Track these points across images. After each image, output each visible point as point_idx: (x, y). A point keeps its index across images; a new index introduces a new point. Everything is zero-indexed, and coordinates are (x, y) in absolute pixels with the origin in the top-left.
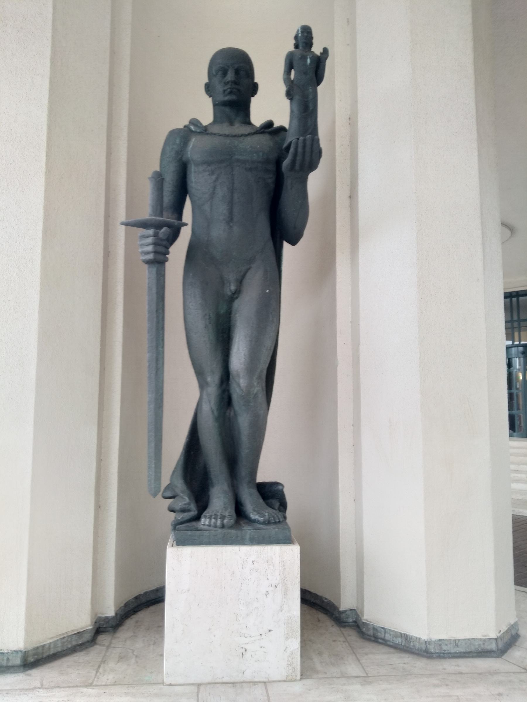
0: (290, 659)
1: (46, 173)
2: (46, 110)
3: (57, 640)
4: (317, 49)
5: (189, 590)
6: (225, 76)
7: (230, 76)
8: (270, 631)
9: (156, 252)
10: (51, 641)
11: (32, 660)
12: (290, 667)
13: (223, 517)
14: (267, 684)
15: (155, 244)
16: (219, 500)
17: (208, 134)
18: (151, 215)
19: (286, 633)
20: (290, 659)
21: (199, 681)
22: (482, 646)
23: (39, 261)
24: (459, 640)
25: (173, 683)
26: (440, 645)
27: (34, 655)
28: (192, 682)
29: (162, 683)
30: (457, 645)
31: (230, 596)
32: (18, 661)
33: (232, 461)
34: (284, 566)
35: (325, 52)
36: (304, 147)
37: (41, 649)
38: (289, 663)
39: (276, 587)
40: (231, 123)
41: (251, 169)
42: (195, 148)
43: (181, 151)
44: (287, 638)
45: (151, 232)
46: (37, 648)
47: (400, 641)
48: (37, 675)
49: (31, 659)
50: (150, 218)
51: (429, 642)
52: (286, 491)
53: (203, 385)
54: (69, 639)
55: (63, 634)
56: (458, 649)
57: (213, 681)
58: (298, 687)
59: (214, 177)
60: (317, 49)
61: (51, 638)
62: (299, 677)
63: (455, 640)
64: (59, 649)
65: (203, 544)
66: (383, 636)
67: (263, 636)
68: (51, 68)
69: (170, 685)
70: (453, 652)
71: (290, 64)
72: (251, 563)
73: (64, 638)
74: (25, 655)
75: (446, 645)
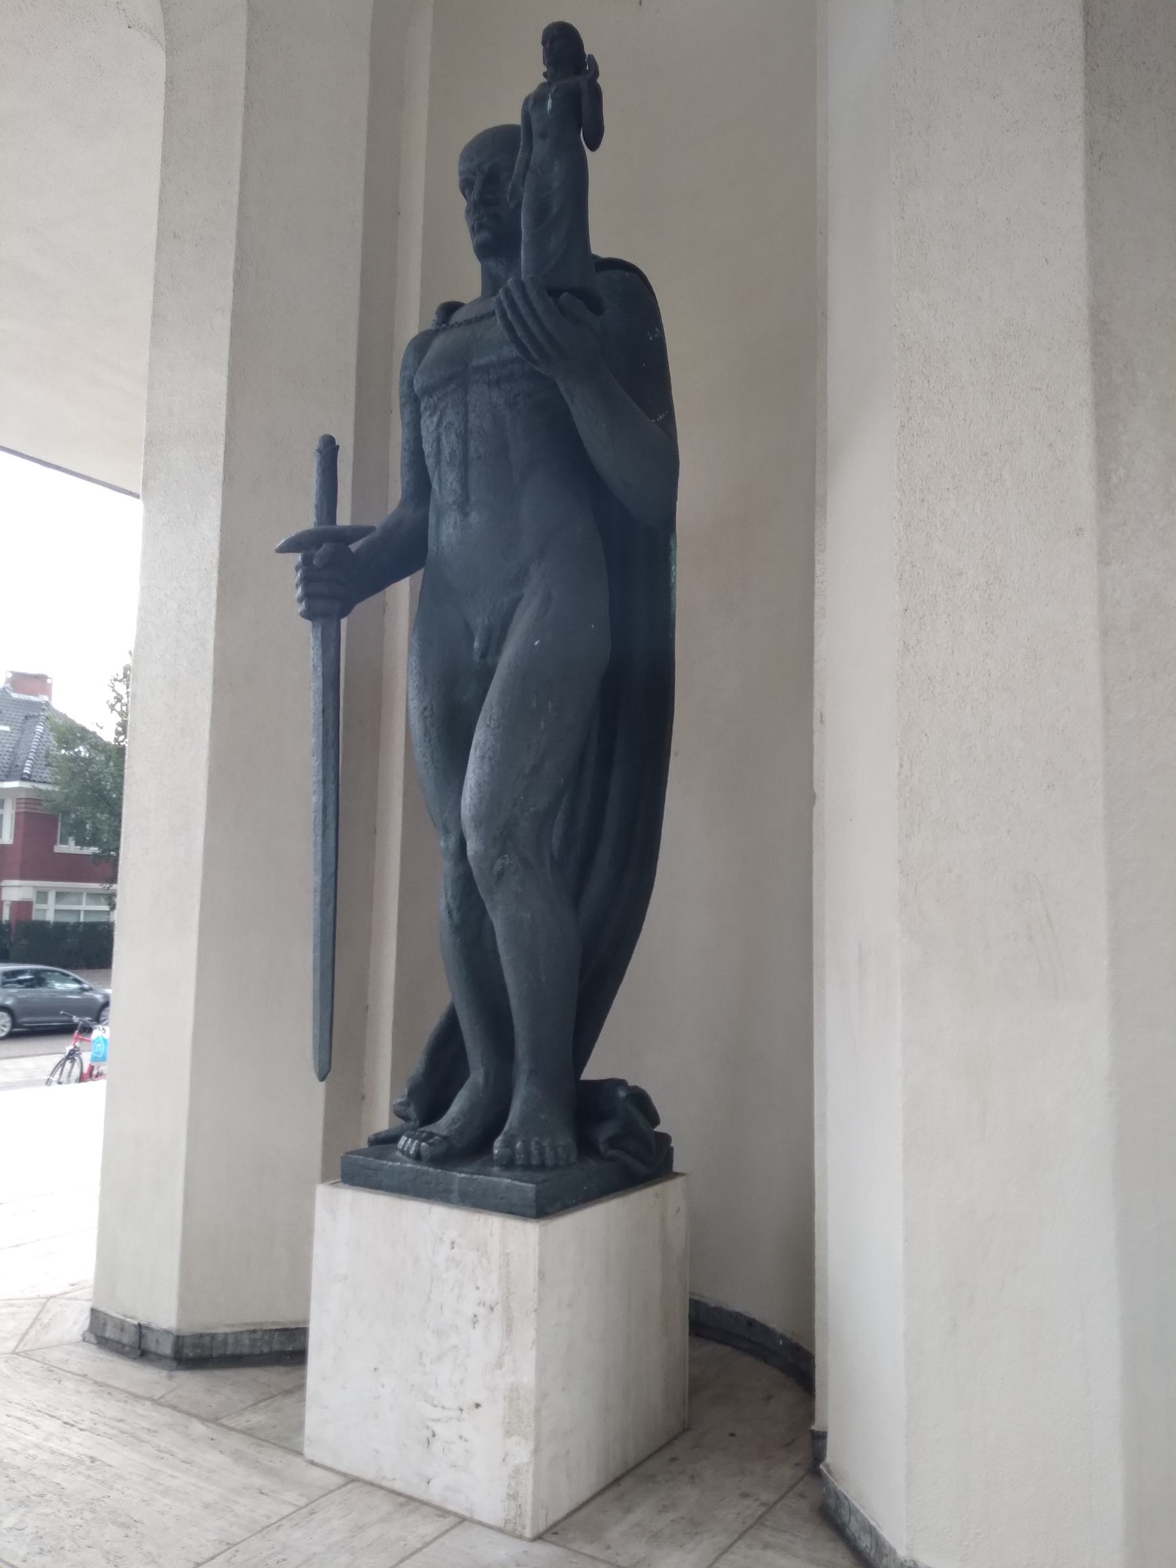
0: (513, 1484)
1: (225, 480)
2: (225, 369)
3: (242, 1333)
8: (478, 1406)
10: (228, 1330)
11: (191, 1355)
12: (513, 1503)
19: (507, 1420)
20: (513, 1484)
21: (354, 1471)
23: (212, 642)
25: (317, 1460)
27: (195, 1346)
28: (343, 1469)
29: (300, 1453)
34: (508, 1265)
36: (513, 304)
37: (207, 1340)
38: (511, 1492)
39: (492, 1309)
41: (498, 382)
44: (508, 1433)
46: (201, 1336)
48: (191, 1385)
49: (189, 1352)
54: (266, 1337)
55: (253, 1324)
57: (377, 1481)
58: (503, 1550)
59: (435, 419)
61: (228, 1325)
64: (246, 1350)
65: (381, 1189)
67: (465, 1414)
69: (312, 1463)
73: (254, 1331)
74: (179, 1341)
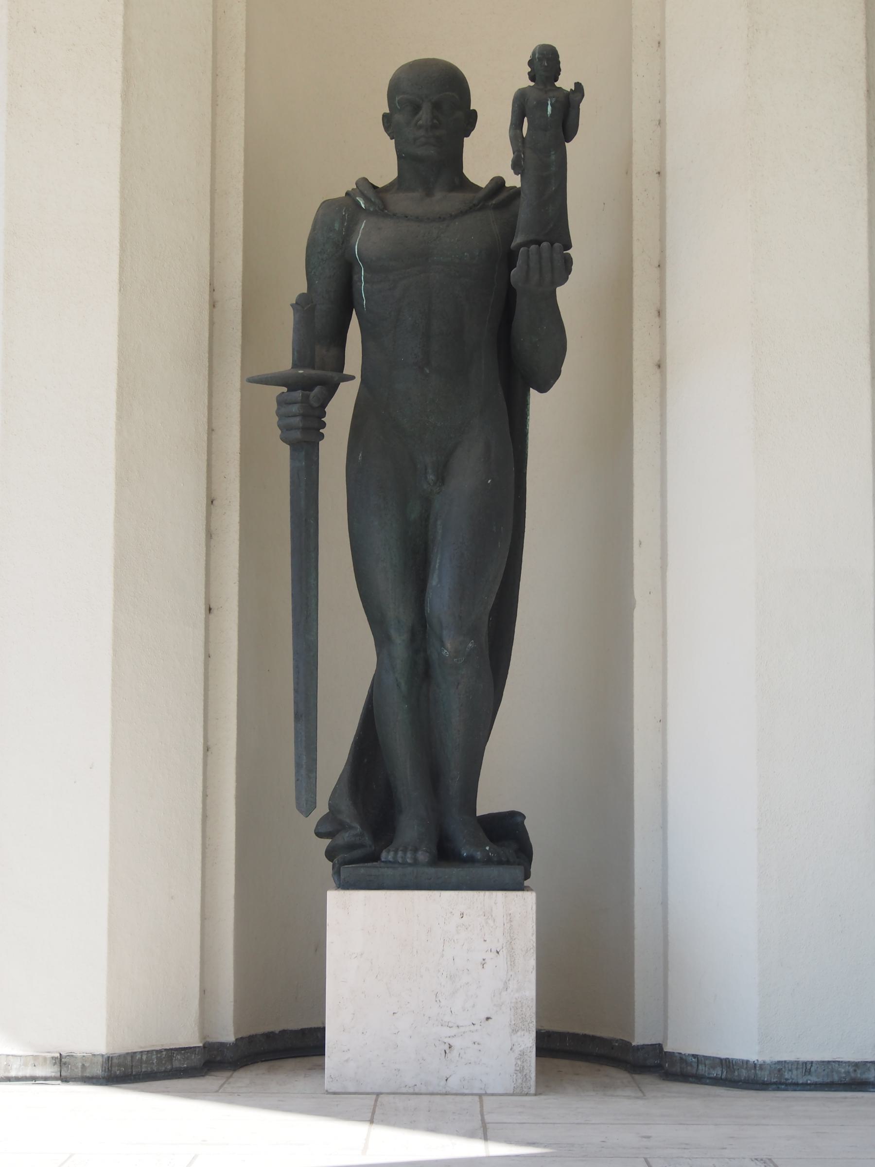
0: (519, 1063)
4: (565, 82)
5: (362, 954)
6: (417, 113)
7: (424, 115)
8: (488, 1019)
9: (305, 429)
13: (415, 850)
14: (485, 1098)
15: (304, 416)
16: (410, 828)
17: (386, 216)
18: (295, 366)
20: (519, 1063)
21: (378, 1091)
22: (853, 1075)
24: (812, 1062)
26: (780, 1070)
30: (808, 1072)
31: (428, 965)
32: (98, 1071)
33: (433, 776)
35: (579, 87)
37: (129, 1059)
40: (429, 192)
42: (367, 238)
43: (343, 243)
44: (515, 1031)
45: (298, 395)
47: (720, 1073)
50: (294, 371)
51: (761, 1065)
52: (529, 824)
53: (382, 640)
56: (809, 1077)
60: (565, 82)
62: (533, 1091)
63: (805, 1063)
66: (694, 1071)
68: (122, 109)
70: (801, 1082)
71: (522, 106)
72: (458, 914)
74: (109, 1060)
75: (790, 1070)
